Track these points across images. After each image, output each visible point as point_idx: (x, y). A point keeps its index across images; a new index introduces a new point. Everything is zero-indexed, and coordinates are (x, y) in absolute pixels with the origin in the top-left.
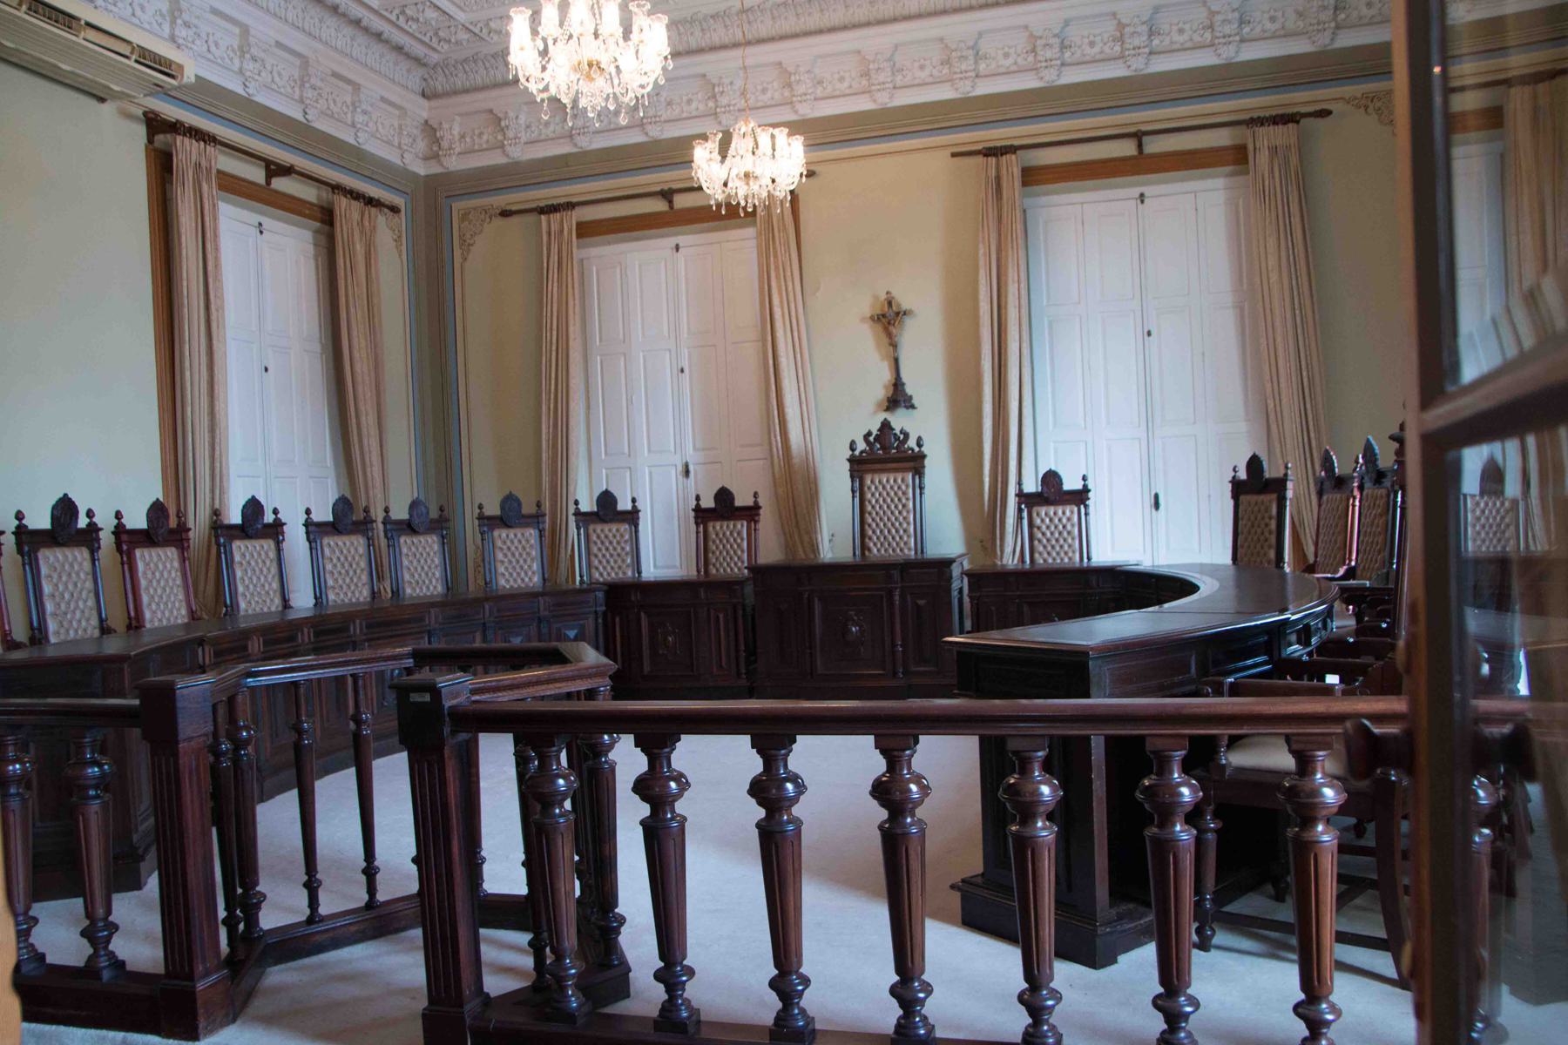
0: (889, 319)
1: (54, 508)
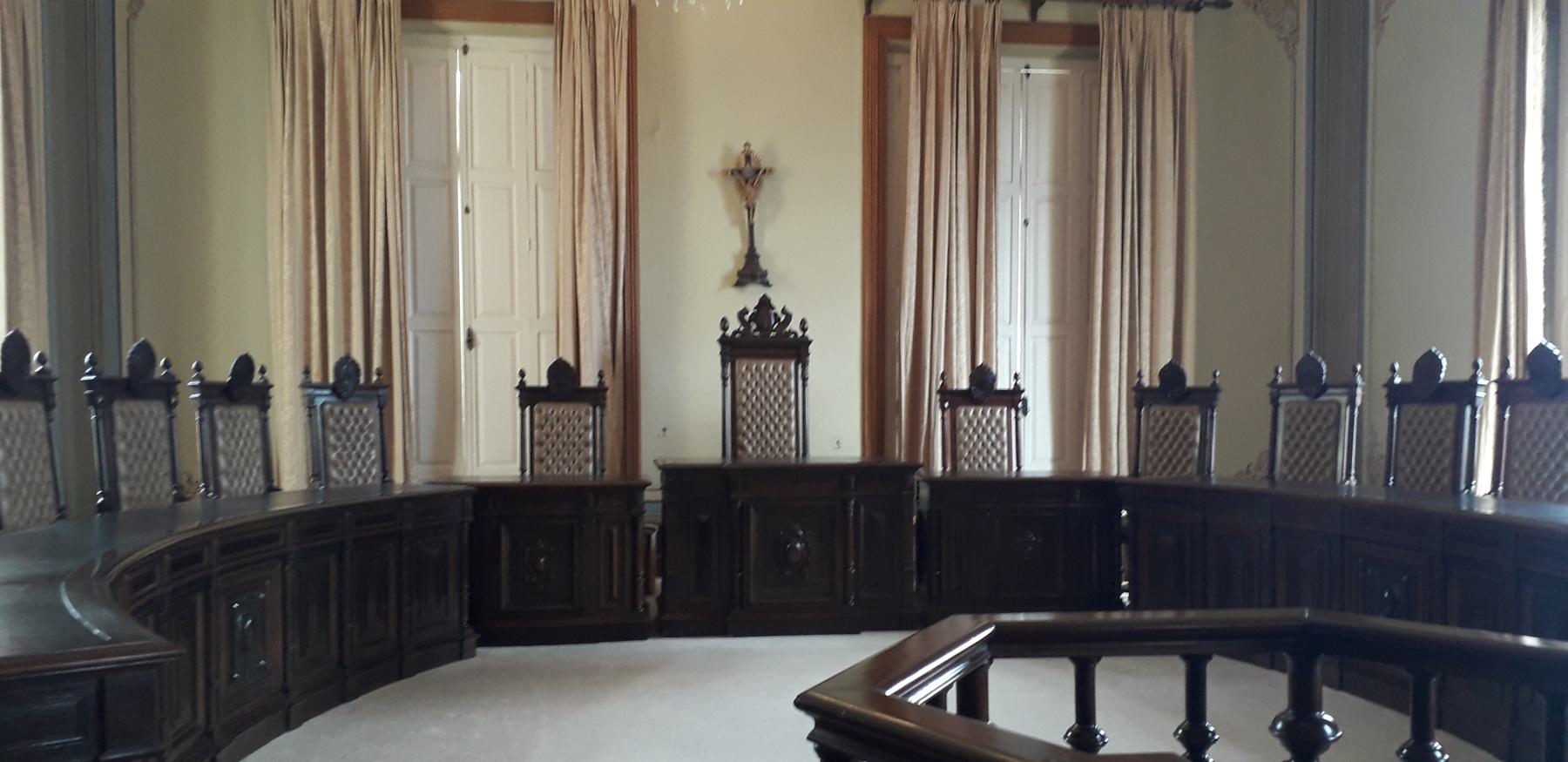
1: (1417, 365)
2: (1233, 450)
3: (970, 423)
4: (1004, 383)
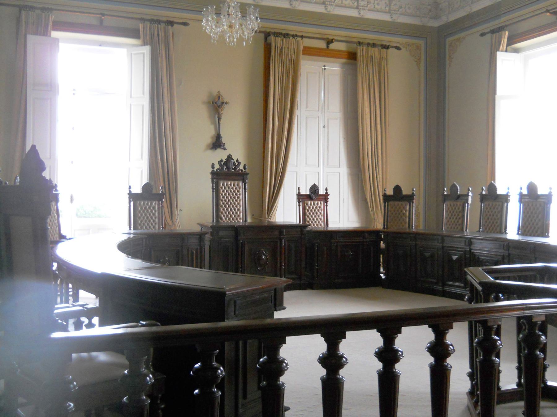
0: (216, 106)
2: (417, 219)
3: (142, 208)
4: (322, 192)
